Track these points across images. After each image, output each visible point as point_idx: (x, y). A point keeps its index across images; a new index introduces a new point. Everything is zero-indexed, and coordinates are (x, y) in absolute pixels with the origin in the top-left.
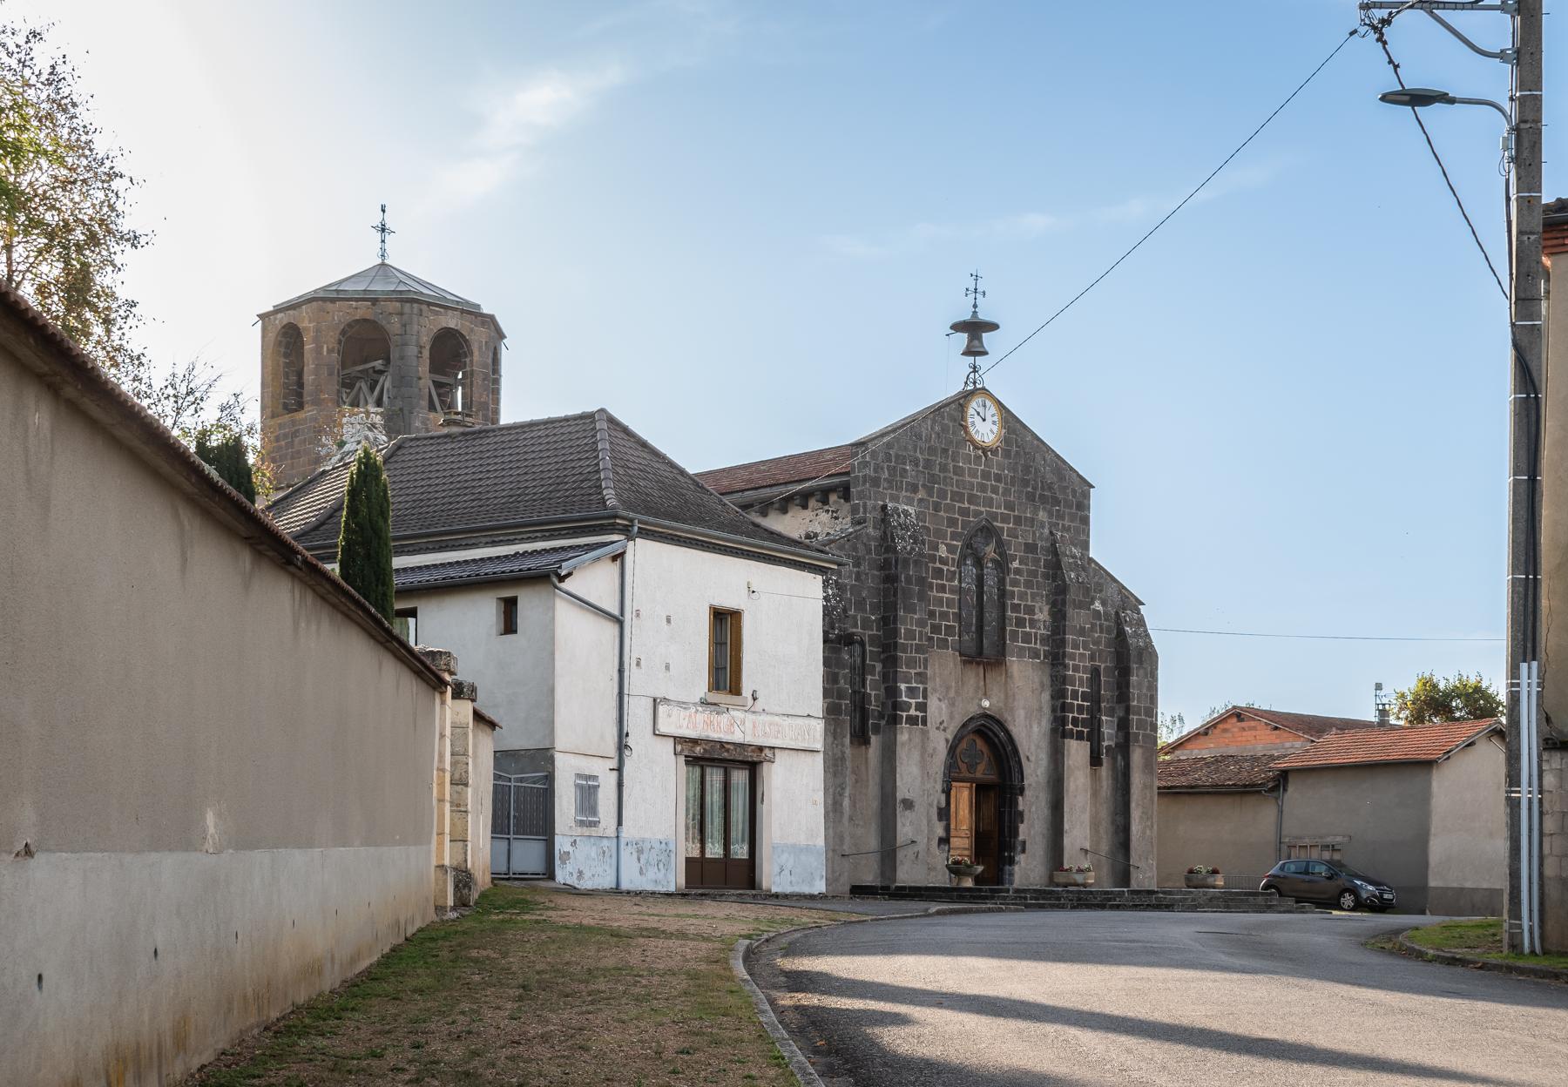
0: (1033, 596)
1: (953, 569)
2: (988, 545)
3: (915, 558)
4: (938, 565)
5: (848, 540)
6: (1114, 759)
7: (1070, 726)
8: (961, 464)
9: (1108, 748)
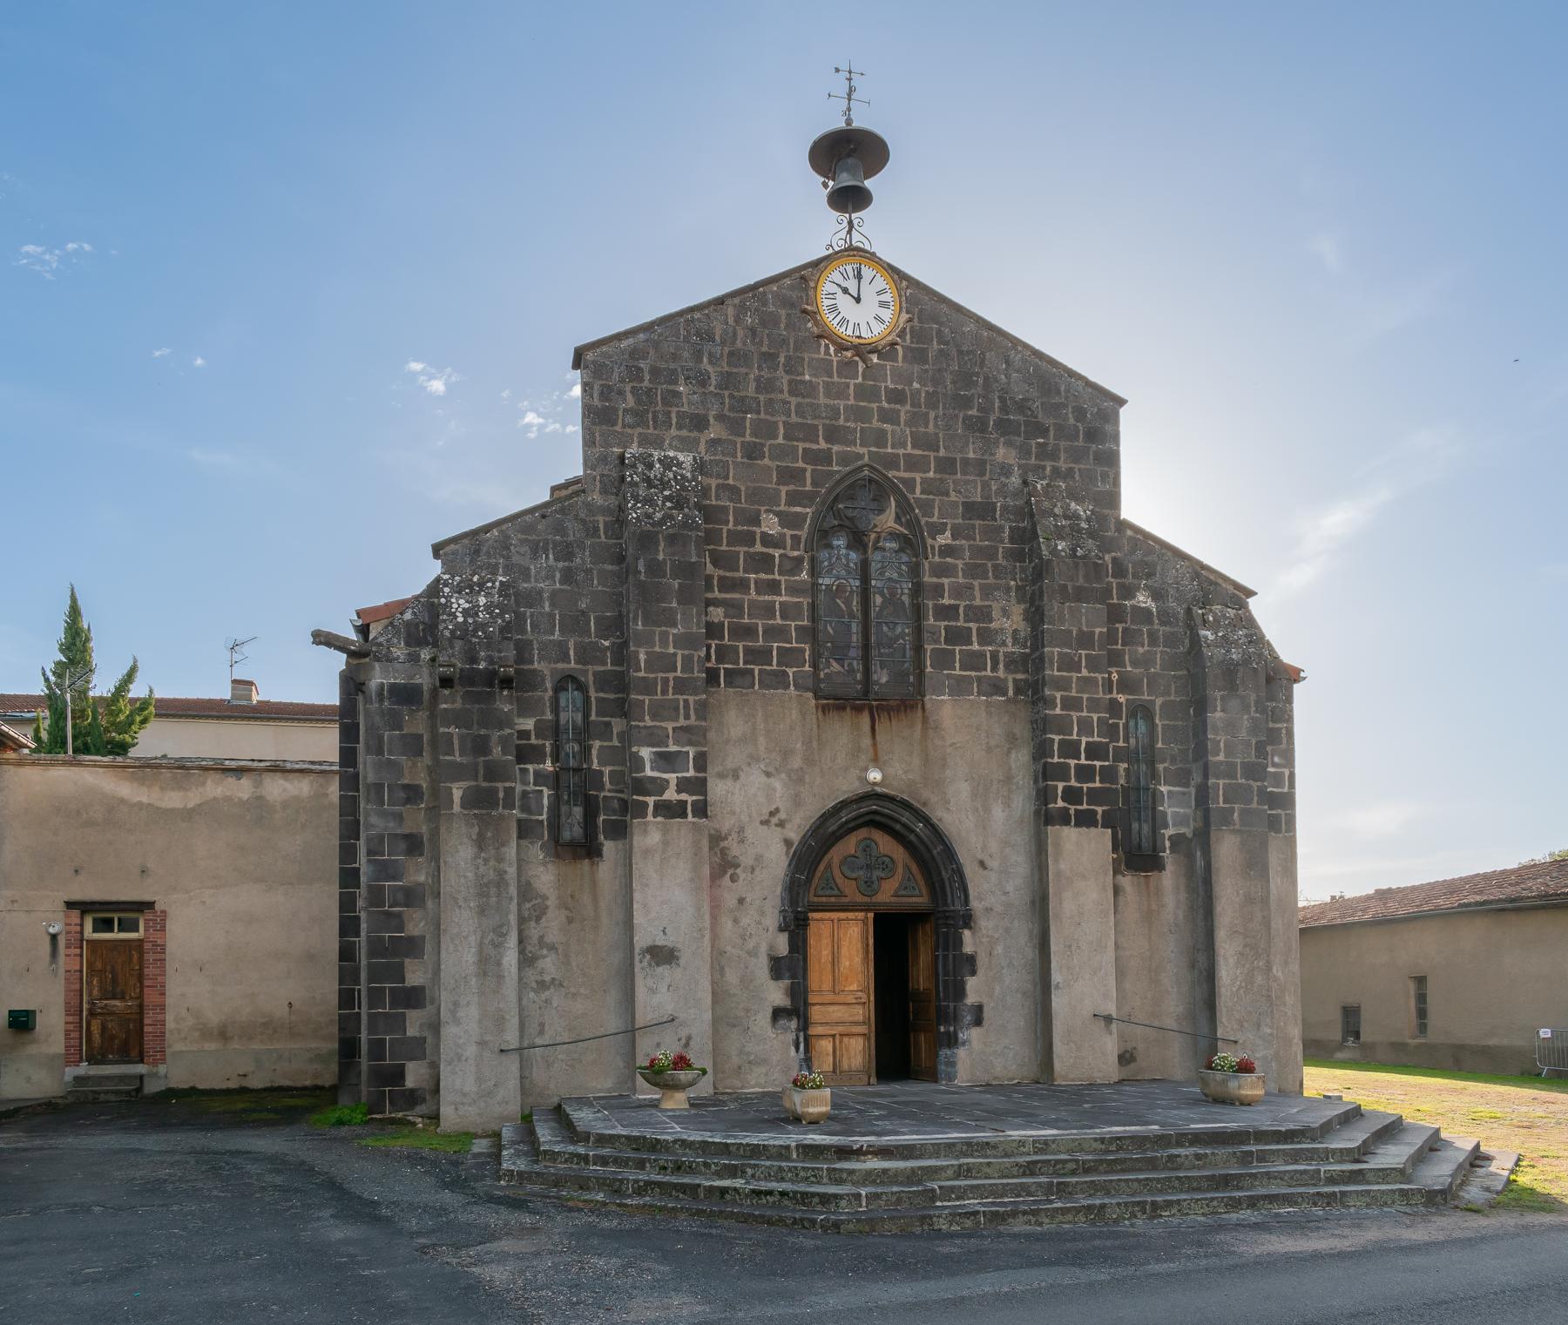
0: (987, 592)
2: (881, 511)
3: (671, 531)
4: (758, 548)
5: (544, 517)
6: (1190, 856)
7: (1060, 804)
8: (807, 377)
9: (1177, 841)
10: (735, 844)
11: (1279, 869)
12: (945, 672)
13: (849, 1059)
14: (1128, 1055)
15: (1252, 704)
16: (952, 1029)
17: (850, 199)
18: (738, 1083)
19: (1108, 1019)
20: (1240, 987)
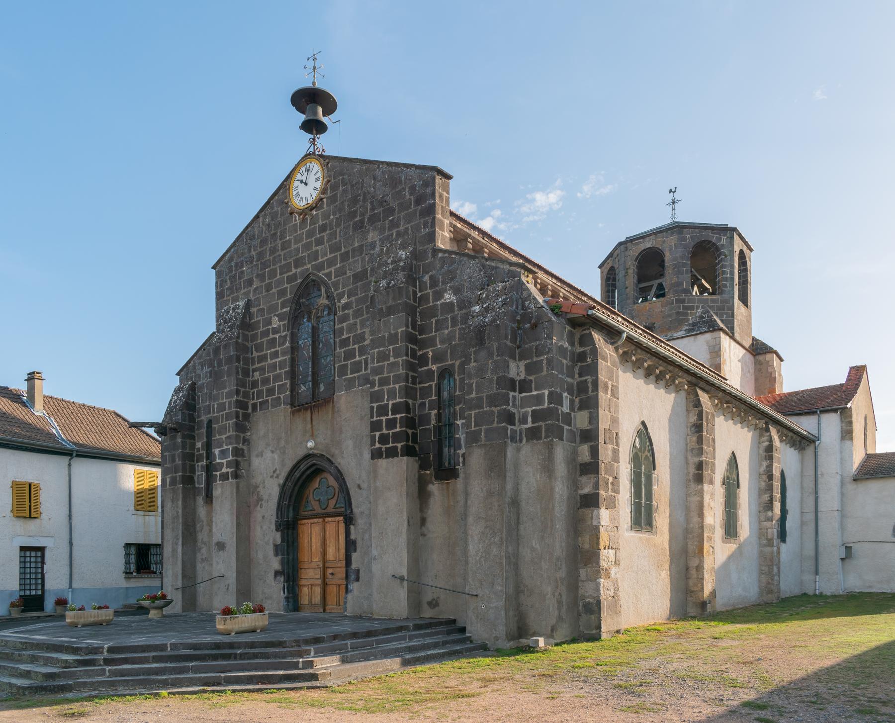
1: (285, 333)
5: (204, 350)
11: (539, 467)
12: (343, 378)
14: (434, 602)
15: (495, 351)
17: (314, 127)
19: (402, 579)
20: (482, 557)
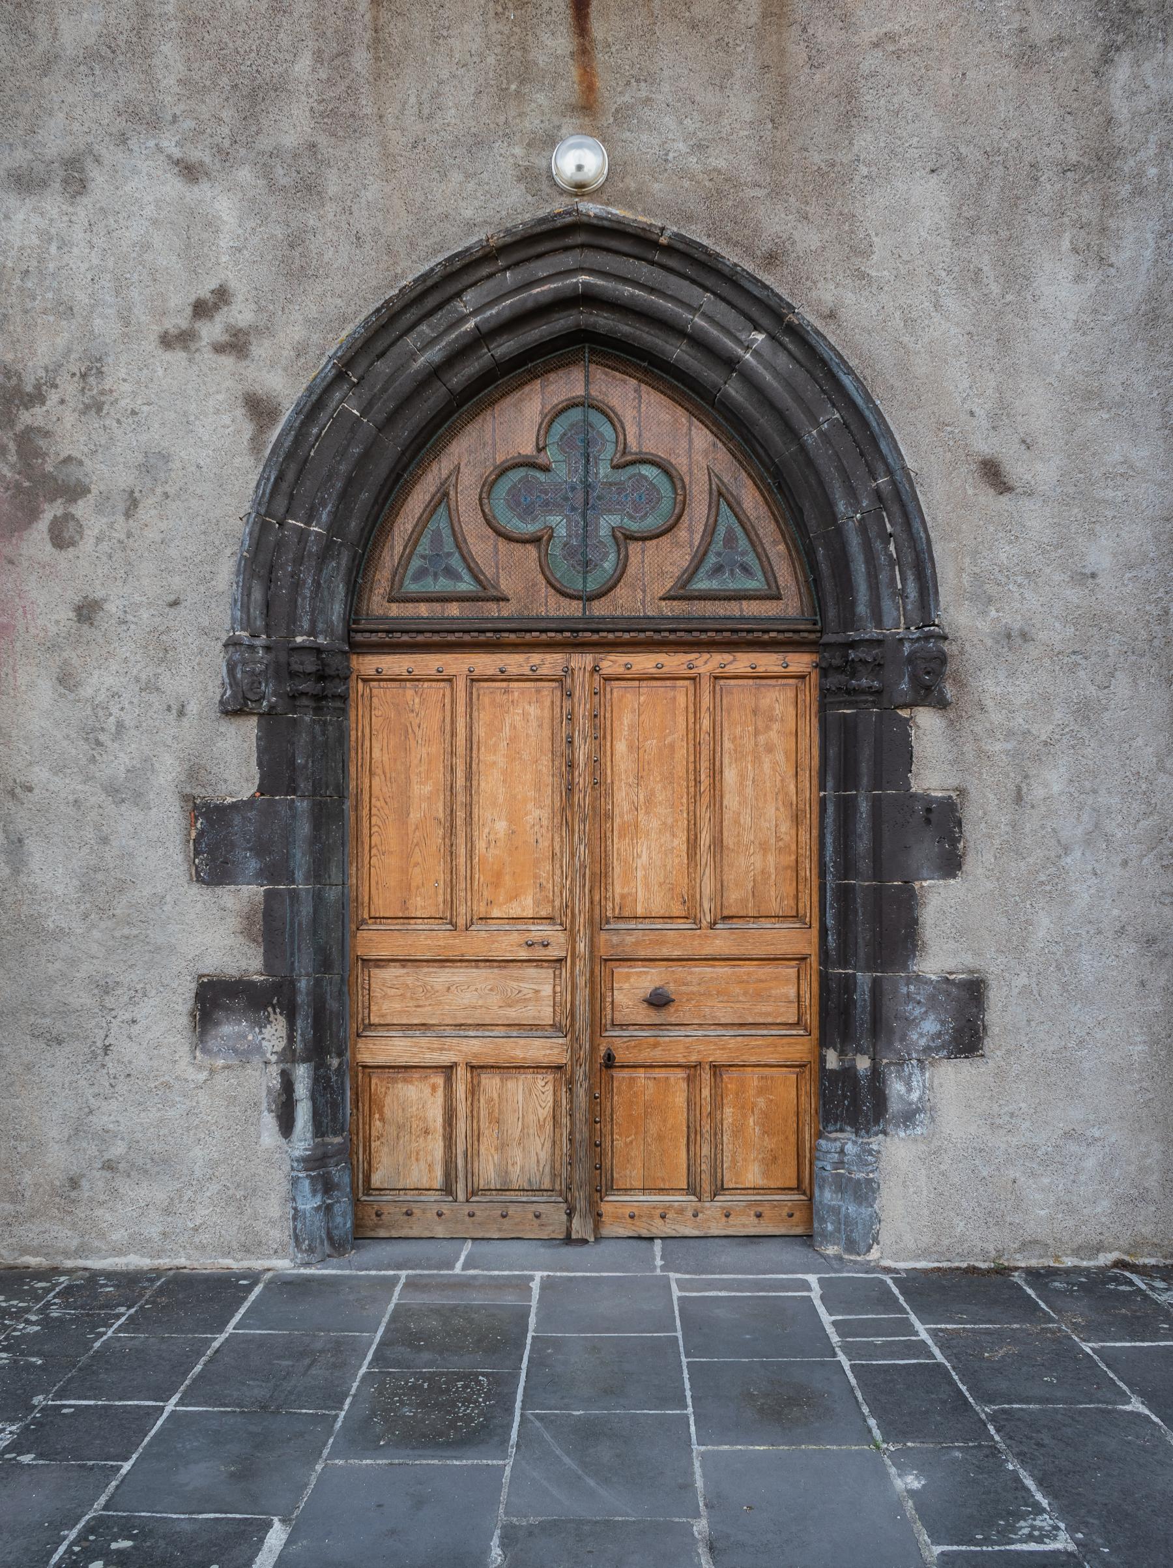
10: (70, 418)
13: (502, 1147)
16: (863, 1064)
18: (63, 1236)
